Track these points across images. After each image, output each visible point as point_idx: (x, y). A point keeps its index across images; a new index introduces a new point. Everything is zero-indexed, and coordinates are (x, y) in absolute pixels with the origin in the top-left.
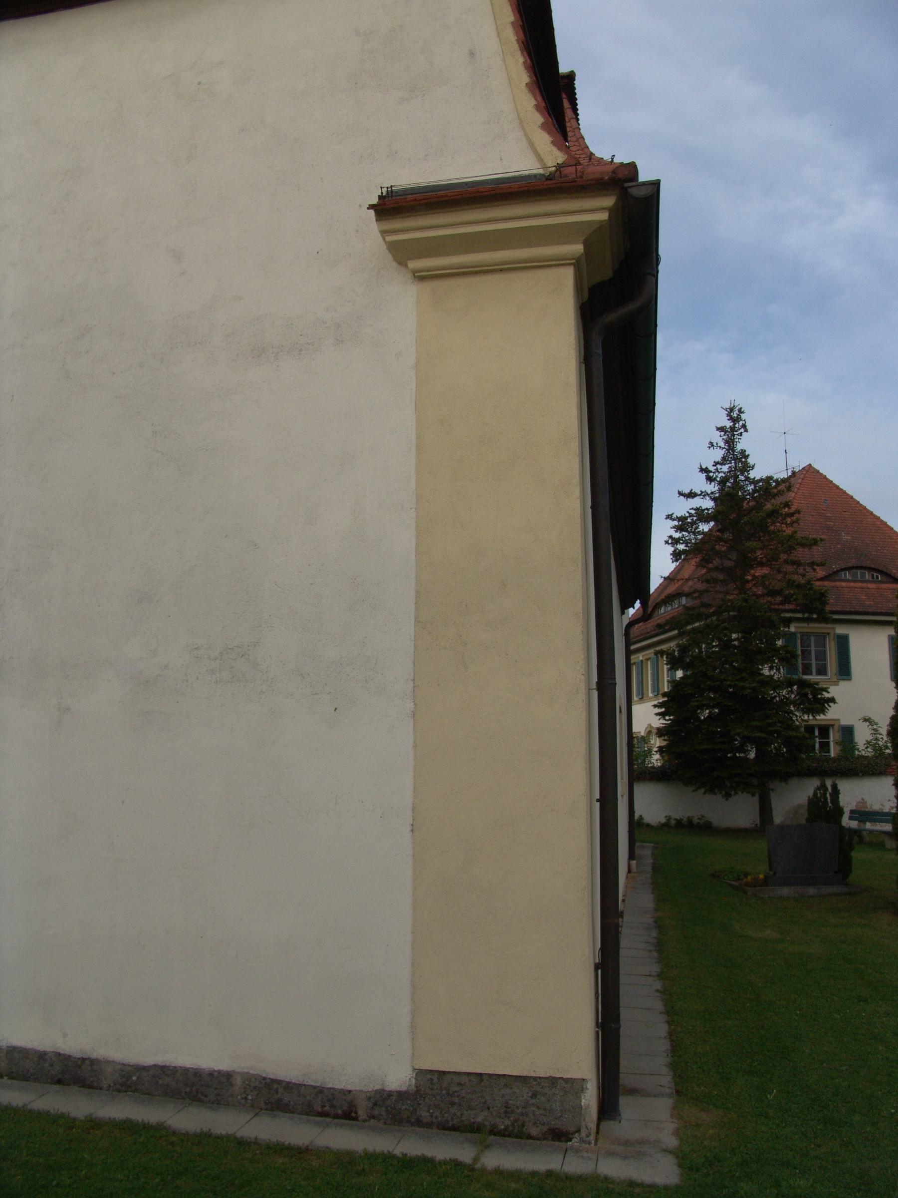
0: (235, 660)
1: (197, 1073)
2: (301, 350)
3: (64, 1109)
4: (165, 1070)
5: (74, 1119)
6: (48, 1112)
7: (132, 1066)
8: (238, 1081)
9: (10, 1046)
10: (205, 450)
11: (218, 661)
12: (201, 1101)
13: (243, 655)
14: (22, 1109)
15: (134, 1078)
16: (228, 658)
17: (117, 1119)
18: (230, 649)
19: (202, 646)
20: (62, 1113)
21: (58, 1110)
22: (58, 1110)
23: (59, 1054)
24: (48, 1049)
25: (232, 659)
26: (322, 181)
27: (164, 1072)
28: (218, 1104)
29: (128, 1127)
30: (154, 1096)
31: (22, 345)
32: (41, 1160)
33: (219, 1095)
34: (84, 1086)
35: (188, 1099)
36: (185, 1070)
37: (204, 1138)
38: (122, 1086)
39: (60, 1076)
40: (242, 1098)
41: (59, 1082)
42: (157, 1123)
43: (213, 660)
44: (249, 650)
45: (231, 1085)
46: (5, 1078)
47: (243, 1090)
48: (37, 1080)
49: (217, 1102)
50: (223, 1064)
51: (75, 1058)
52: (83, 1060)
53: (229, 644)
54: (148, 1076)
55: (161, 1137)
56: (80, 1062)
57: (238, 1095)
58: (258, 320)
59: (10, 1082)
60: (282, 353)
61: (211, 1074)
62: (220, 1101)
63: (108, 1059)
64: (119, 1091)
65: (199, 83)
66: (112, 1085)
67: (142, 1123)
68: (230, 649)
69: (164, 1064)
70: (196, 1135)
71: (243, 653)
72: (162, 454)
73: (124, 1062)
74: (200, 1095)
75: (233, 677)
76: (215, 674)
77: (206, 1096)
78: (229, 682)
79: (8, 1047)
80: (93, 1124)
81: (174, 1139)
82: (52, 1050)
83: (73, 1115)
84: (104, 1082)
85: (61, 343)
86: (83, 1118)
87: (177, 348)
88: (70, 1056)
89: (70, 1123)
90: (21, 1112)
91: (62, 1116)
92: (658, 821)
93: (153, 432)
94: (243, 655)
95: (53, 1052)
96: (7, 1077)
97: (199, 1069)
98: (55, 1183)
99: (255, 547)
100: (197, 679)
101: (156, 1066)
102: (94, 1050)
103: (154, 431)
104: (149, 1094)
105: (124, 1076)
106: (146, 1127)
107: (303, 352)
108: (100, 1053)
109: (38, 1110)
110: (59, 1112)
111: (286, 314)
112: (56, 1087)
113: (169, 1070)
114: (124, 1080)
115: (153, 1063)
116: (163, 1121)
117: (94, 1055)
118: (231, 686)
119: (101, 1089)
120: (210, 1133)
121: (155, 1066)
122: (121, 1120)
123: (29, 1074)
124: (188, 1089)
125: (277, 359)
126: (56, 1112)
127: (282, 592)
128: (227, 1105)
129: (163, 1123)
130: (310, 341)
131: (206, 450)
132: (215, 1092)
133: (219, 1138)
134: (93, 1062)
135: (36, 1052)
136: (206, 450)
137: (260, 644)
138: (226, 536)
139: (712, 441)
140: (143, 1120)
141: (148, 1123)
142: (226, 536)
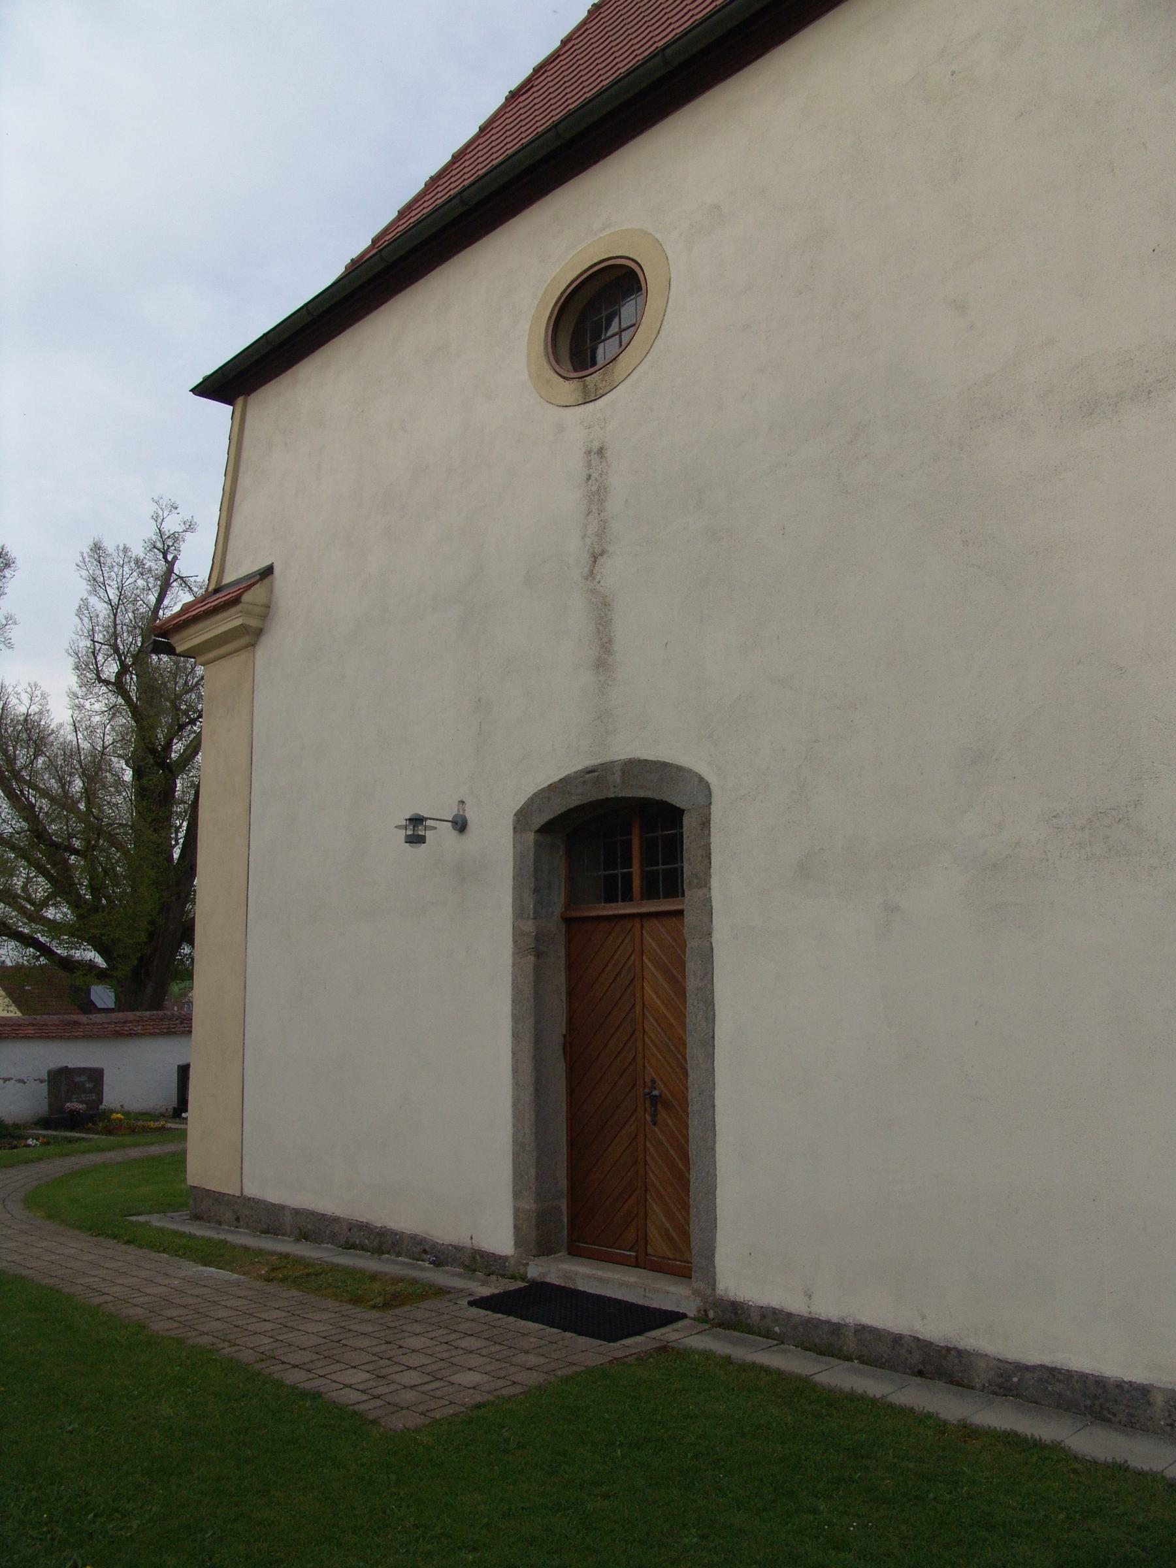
0: (1109, 827)
1: (1100, 1382)
2: (1150, 392)
3: (931, 1408)
4: (1055, 1373)
5: (945, 1423)
6: (912, 1408)
7: (1010, 1363)
8: (1159, 1399)
9: (859, 1323)
10: (1035, 553)
11: (1087, 830)
12: (1105, 1420)
13: (1120, 820)
14: (880, 1400)
15: (1015, 1379)
16: (1100, 825)
17: (998, 1429)
18: (1101, 813)
19: (1063, 813)
20: (929, 1413)
21: (924, 1407)
22: (924, 1407)
23: (918, 1339)
24: (905, 1332)
25: (1106, 826)
26: (1146, 148)
27: (1054, 1376)
28: (1132, 1427)
29: (1012, 1440)
30: (1043, 1405)
31: (786, 465)
32: (912, 1465)
33: (1132, 1415)
34: (951, 1382)
35: (1090, 1416)
36: (1083, 1377)
37: (1119, 1470)
38: (1000, 1388)
39: (921, 1367)
40: (1168, 1425)
41: (920, 1374)
42: (1052, 1442)
43: (1079, 830)
44: (1128, 812)
45: (1149, 1404)
46: (856, 1361)
47: (1167, 1414)
48: (893, 1368)
49: (1131, 1424)
50: (1137, 1374)
51: (937, 1346)
52: (948, 1349)
53: (1100, 807)
54: (1033, 1378)
55: (1058, 1461)
56: (944, 1352)
57: (1160, 1420)
58: (1082, 365)
59: (861, 1366)
60: (1123, 403)
61: (1120, 1385)
62: (1135, 1423)
63: (980, 1352)
64: (996, 1394)
65: (953, 73)
66: (987, 1385)
67: (1031, 1438)
68: (1101, 813)
69: (1054, 1366)
70: (1106, 1465)
71: (1120, 817)
72: (979, 567)
73: (999, 1357)
74: (1105, 1412)
75: (1110, 849)
76: (1084, 849)
77: (1115, 1415)
78: (1104, 857)
79: (855, 1325)
80: (969, 1431)
81: (1078, 1466)
82: (910, 1333)
83: (943, 1416)
84: (977, 1380)
85: (832, 452)
86: (955, 1422)
87: (979, 426)
88: (931, 1343)
89: (942, 1427)
90: (879, 1405)
91: (929, 1416)
92: (912, 1406)
93: (963, 541)
94: (1120, 820)
95: (910, 1336)
96: (858, 1361)
97: (1102, 1376)
98: (931, 1496)
99: (1121, 672)
100: (1061, 857)
101: (1042, 1367)
102: (961, 1339)
103: (965, 540)
104: (1036, 1403)
105: (1002, 1375)
106: (1037, 1445)
107: (1152, 394)
108: (970, 1342)
109: (900, 1405)
110: (925, 1411)
111: (1121, 348)
112: (919, 1380)
113: (1060, 1373)
114: (1001, 1380)
115: (1039, 1363)
116: (1058, 1440)
117: (962, 1345)
118: (1109, 862)
119: (973, 1388)
120: (1126, 1465)
121: (1042, 1366)
122: (1005, 1431)
123: (884, 1360)
124: (1088, 1402)
125: (1117, 412)
126: (921, 1410)
127: (1166, 728)
128: (1145, 1431)
129: (1059, 1443)
130: (1160, 377)
131: (1037, 552)
132: (1127, 1411)
133: (1140, 1474)
134: (960, 1353)
135: (889, 1334)
136: (1037, 552)
137: (1143, 802)
138: (1079, 663)
139: (205, 677)
140: (1032, 1435)
141: (1040, 1440)
142: (1079, 663)
